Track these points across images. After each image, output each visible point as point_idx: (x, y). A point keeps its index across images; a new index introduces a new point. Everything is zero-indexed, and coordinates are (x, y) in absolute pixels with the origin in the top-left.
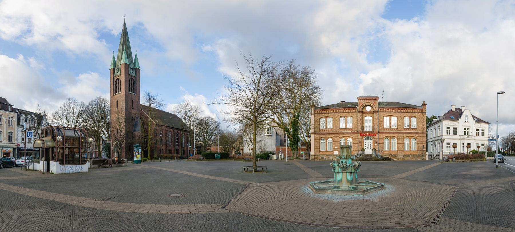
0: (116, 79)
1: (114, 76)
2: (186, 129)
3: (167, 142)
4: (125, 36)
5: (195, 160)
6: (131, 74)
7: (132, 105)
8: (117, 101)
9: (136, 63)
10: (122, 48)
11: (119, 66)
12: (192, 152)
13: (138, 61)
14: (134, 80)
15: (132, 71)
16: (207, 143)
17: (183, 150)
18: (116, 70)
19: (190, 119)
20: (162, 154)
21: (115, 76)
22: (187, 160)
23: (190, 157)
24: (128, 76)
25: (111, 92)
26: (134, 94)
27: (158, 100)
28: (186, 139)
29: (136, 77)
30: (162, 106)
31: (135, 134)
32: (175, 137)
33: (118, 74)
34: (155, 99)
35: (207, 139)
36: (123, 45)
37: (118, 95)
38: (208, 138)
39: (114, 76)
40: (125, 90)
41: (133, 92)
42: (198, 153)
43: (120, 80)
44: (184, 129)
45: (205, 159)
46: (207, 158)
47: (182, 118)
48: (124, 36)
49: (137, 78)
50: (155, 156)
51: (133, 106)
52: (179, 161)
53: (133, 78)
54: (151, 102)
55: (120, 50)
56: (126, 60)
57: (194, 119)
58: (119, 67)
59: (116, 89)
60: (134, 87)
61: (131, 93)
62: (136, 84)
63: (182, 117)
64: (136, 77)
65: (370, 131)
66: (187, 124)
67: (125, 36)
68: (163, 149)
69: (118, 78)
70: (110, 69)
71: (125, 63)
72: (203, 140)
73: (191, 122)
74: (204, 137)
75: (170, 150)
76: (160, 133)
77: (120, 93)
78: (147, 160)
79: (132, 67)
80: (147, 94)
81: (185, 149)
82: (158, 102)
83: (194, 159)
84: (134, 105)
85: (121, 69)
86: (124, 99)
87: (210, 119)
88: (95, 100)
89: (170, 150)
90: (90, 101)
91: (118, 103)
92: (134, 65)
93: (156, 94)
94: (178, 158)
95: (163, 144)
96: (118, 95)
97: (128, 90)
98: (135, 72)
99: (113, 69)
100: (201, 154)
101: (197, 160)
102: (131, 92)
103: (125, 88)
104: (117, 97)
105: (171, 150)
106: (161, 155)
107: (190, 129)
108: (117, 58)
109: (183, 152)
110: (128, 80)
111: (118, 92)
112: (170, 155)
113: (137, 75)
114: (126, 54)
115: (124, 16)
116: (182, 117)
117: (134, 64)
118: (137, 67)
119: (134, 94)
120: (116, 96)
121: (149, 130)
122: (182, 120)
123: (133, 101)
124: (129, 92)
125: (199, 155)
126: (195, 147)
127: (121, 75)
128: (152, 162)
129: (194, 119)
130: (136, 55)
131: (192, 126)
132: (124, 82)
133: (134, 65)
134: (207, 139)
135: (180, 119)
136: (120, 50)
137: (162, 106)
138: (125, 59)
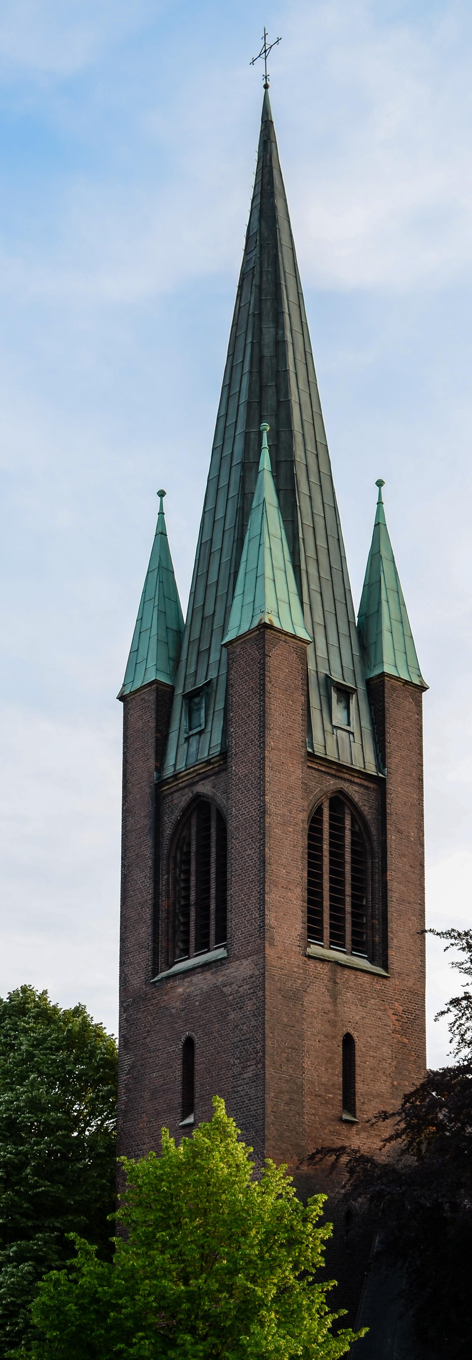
1: (160, 768)
6: (332, 755)
10: (241, 429)
11: (214, 656)
14: (358, 816)
21: (169, 772)
26: (364, 964)
33: (204, 755)
41: (358, 947)
70: (121, 698)
84: (360, 1087)
98: (366, 723)
102: (337, 941)
104: (187, 998)
113: (393, 761)
123: (348, 1042)
124: (314, 950)
130: (379, 527)
136: (223, 483)
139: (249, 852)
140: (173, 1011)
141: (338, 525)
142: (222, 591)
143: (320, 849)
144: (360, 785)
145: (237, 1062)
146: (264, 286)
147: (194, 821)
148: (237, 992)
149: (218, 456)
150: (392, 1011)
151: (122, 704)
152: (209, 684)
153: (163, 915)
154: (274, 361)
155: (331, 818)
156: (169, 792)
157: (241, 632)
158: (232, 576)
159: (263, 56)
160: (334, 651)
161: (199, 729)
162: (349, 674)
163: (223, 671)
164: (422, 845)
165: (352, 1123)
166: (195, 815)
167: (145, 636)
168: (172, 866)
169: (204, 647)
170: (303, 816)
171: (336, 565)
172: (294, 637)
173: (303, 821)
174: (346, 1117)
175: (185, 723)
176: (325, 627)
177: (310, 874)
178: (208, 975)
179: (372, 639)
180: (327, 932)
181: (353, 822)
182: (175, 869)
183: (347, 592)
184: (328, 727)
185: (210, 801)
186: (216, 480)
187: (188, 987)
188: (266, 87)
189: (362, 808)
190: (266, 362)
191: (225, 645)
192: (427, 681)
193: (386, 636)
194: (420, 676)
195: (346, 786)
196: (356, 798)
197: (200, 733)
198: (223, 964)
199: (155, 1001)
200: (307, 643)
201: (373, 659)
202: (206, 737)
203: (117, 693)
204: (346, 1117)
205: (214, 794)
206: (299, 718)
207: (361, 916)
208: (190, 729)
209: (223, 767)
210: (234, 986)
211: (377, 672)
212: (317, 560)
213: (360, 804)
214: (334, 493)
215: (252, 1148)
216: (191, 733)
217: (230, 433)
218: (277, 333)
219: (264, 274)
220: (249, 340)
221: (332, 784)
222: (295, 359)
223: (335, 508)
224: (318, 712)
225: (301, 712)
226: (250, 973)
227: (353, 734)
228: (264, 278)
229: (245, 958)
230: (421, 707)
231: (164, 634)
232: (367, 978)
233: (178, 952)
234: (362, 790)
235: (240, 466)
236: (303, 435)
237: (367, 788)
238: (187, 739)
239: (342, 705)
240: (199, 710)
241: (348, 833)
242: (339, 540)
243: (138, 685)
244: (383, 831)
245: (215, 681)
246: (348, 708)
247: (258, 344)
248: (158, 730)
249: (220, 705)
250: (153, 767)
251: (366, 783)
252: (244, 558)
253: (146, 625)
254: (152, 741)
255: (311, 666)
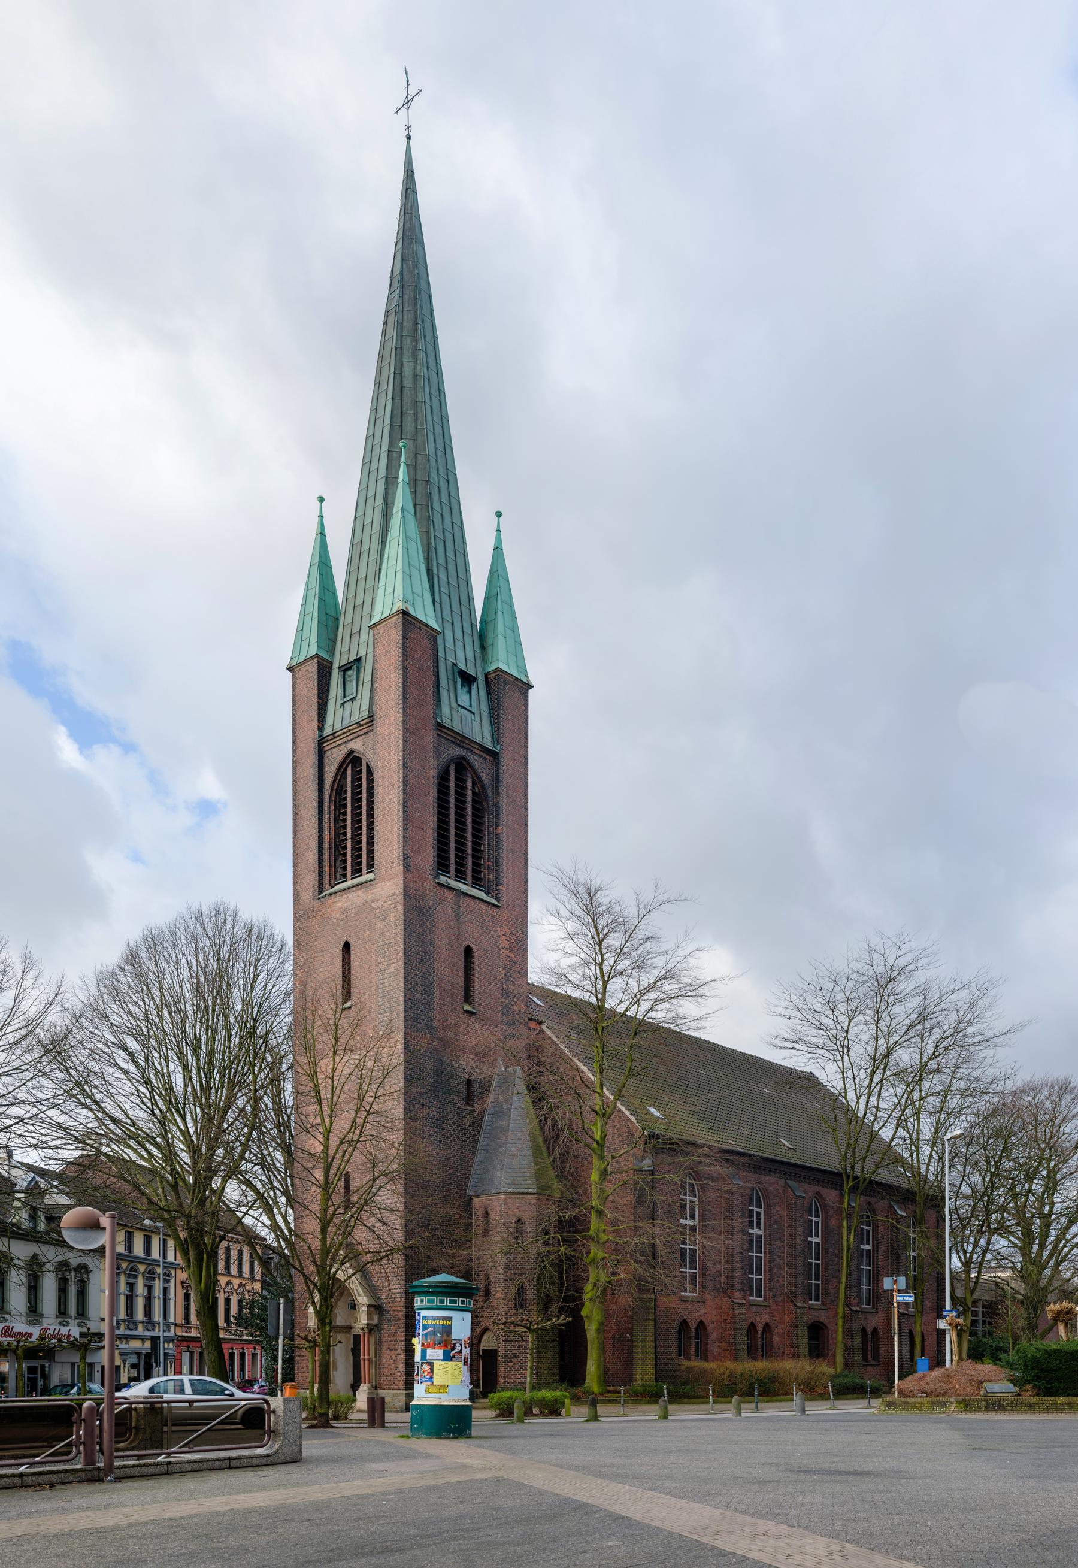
0: (335, 756)
1: (321, 729)
2: (885, 1176)
3: (738, 1274)
4: (407, 342)
5: (943, 1405)
6: (457, 727)
7: (461, 981)
8: (347, 947)
9: (500, 627)
10: (385, 447)
11: (364, 638)
12: (930, 1343)
13: (511, 605)
14: (477, 781)
15: (463, 698)
16: (1051, 1279)
17: (864, 1330)
18: (335, 674)
19: (916, 1095)
20: (697, 1364)
21: (328, 731)
22: (877, 1402)
23: (910, 1383)
24: (429, 737)
25: (301, 866)
26: (482, 895)
27: (664, 947)
28: (882, 1248)
29: (495, 755)
30: (694, 990)
31: (487, 1213)
32: (800, 1230)
33: (355, 718)
34: (641, 934)
35: (1046, 1253)
36: (397, 430)
37: (351, 895)
38: (1058, 1239)
39: (321, 729)
40: (406, 858)
41: (477, 882)
42: (976, 1354)
43: (370, 772)
44: (867, 1169)
45: (1027, 1397)
46: (1050, 1392)
47: (851, 1095)
48: (401, 337)
49: (506, 760)
50: (644, 1374)
51: (468, 997)
52: (817, 1409)
53: (476, 761)
54: (610, 959)
55: (334, 745)
56: (418, 590)
57: (946, 1094)
58: (362, 653)
59: (338, 847)
60: (476, 845)
61: (453, 883)
62: (497, 816)
63: (850, 1084)
64: (495, 755)
65: (330, 1394)
66: (886, 1134)
67: (407, 342)
68: (701, 1325)
69: (351, 752)
70: (290, 669)
71: (405, 613)
72: (1018, 1260)
73: (917, 1114)
74: (1028, 1237)
75: (760, 1329)
76: (683, 1207)
77: (365, 877)
78: (567, 1401)
79: (464, 657)
80: (576, 894)
81: (873, 1322)
82: (660, 962)
83: (937, 1398)
84: (477, 986)
85: (380, 673)
86: (401, 928)
87: (1068, 1098)
88: (173, 933)
89: (760, 1329)
90: (134, 934)
91: (355, 964)
92: (483, 648)
93: (647, 897)
94: (812, 1390)
95: (704, 1286)
96: (355, 898)
97: (429, 857)
98: (484, 707)
99: (313, 668)
100: (996, 1359)
101: (967, 1405)
102: (460, 875)
103: (406, 839)
104: (345, 911)
105: (767, 1327)
106: (686, 1363)
107: (916, 1171)
108: (347, 586)
109: (858, 1339)
110: (432, 774)
111: (357, 871)
112: (760, 1366)
113: (506, 739)
114: (410, 518)
115: (408, 102)
116: (850, 1084)
117: (483, 641)
118: (501, 661)
119: (482, 895)
120: (341, 903)
121: (595, 1177)
122: (853, 1104)
123: (468, 951)
124: (443, 879)
125: (985, 1368)
126: (948, 1306)
127: (378, 723)
128: (595, 1418)
129: (946, 1094)
130: (498, 549)
131: (926, 1150)
132: (400, 784)
133: (483, 648)
134: (1046, 1253)
135: (833, 1102)
136: (371, 493)
137: (694, 990)
138: (409, 576)
139: (390, 797)
140: (335, 921)
141: (464, 544)
142: (370, 584)
143: (448, 802)
144: (480, 756)
145: (383, 960)
146: (405, 324)
147: (349, 772)
148: (383, 906)
149: (366, 471)
150: (502, 933)
151: (290, 674)
152: (359, 660)
153: (326, 846)
154: (413, 392)
155: (456, 778)
156: (329, 747)
157: (384, 617)
158: (377, 572)
159: (406, 106)
160: (459, 644)
161: (351, 697)
162: (471, 666)
163: (370, 649)
164: (527, 809)
165: (472, 1013)
166: (350, 767)
167: (308, 618)
168: (333, 807)
169: (356, 629)
170: (433, 773)
171: (462, 575)
172: (427, 625)
173: (434, 777)
174: (467, 1007)
175: (340, 691)
176: (452, 624)
177: (439, 820)
178: (360, 893)
179: (490, 641)
180: (452, 868)
181: (474, 784)
182: (335, 810)
183: (470, 599)
184: (454, 704)
185: (360, 756)
186: (365, 491)
187: (346, 902)
188: (409, 137)
189: (481, 774)
190: (406, 392)
191: (371, 627)
192: (532, 680)
193: (501, 639)
194: (527, 676)
195: (468, 754)
196: (477, 765)
197: (353, 699)
198: (371, 885)
199: (320, 913)
200: (439, 633)
201: (490, 657)
202: (356, 703)
203: (286, 664)
204: (467, 1007)
205: (364, 750)
206: (430, 693)
207: (480, 858)
208: (345, 697)
209: (371, 728)
210: (380, 902)
211: (493, 667)
212: (447, 569)
213: (479, 771)
214: (461, 516)
215: (7, 1366)
216: (345, 700)
217: (376, 452)
218: (415, 368)
219: (405, 312)
220: (392, 370)
221: (457, 751)
222: (430, 393)
223: (462, 529)
224: (446, 692)
225: (432, 688)
226: (392, 892)
227: (474, 713)
228: (405, 317)
229: (389, 880)
230: (527, 700)
231: (324, 618)
232: (482, 906)
233: (338, 876)
234: (480, 760)
235: (384, 480)
236: (437, 461)
237: (485, 759)
238: (342, 704)
239: (466, 689)
240: (351, 681)
241: (469, 793)
242: (465, 556)
243: (302, 658)
244: (497, 793)
245: (363, 658)
246: (470, 692)
247: (399, 374)
248: (319, 697)
249: (368, 678)
250: (316, 727)
251: (484, 755)
252: (386, 556)
253: (309, 609)
254: (315, 706)
255: (441, 654)
